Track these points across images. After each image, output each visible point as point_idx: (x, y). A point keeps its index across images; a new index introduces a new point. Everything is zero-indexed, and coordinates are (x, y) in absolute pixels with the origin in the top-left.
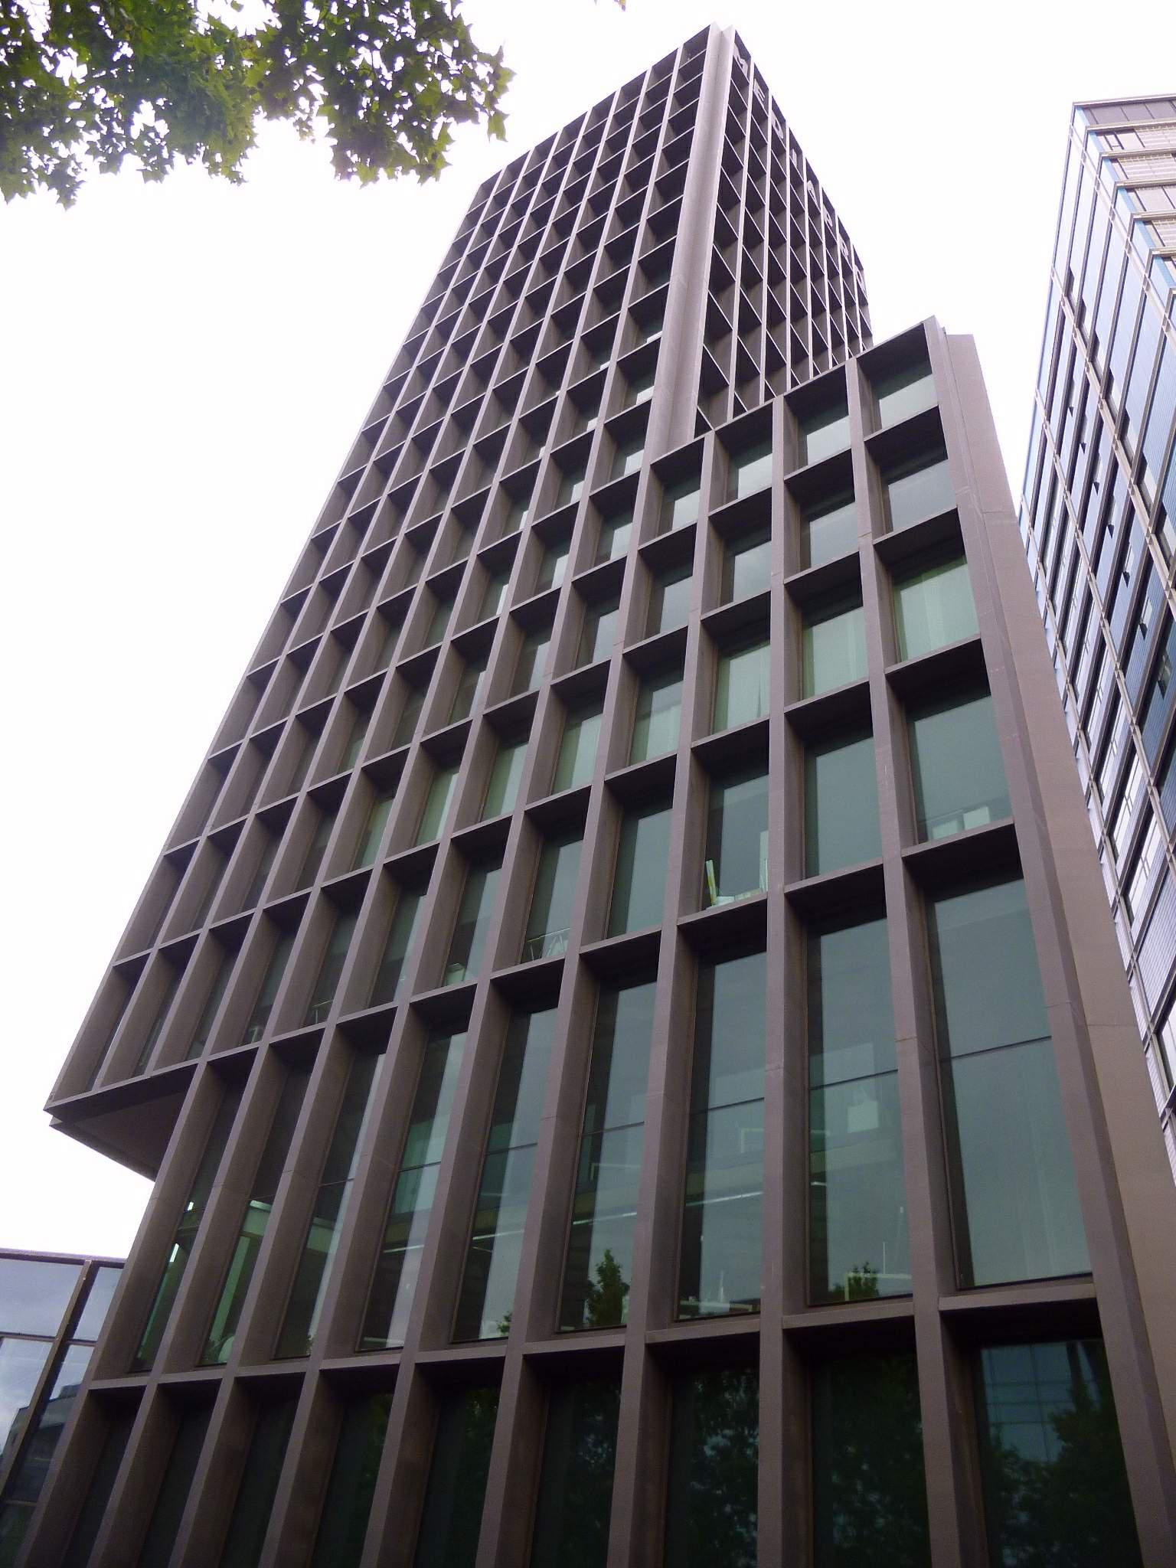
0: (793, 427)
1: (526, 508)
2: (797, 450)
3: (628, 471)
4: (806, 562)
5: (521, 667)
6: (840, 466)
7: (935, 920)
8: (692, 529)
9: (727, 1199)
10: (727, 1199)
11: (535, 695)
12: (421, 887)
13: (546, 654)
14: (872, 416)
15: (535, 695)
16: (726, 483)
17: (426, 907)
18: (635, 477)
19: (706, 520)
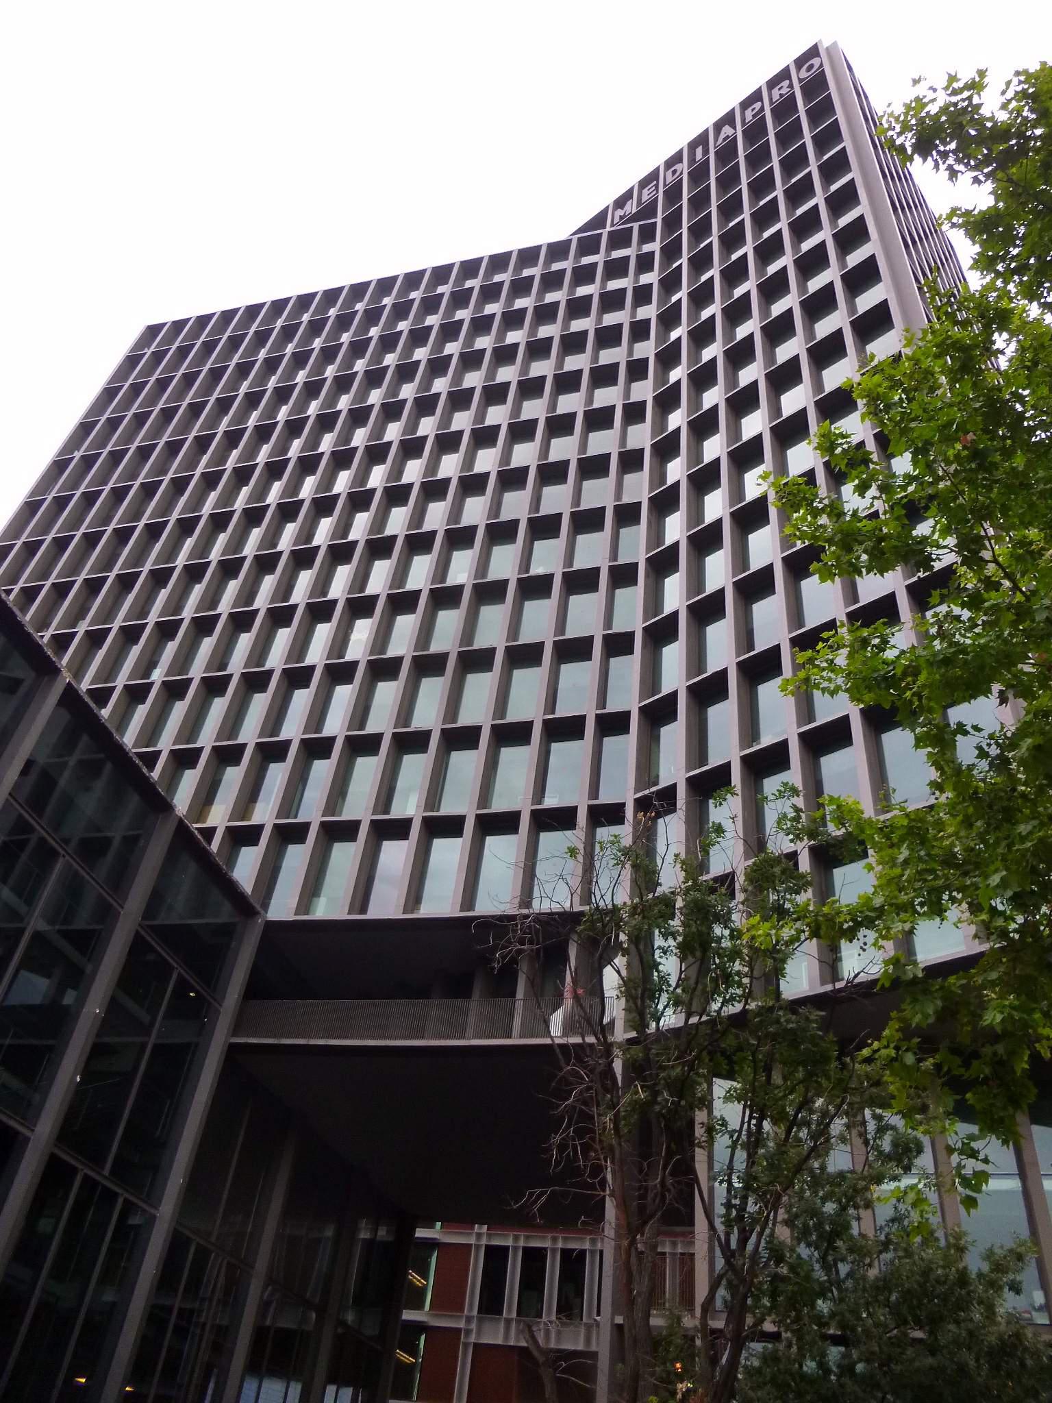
0: (726, 287)
1: (191, 536)
2: (810, 333)
3: (399, 329)
4: (497, 515)
5: (283, 448)
6: (800, 417)
7: (330, 853)
8: (677, 544)
9: (24, 1329)
10: (24, 1329)
11: (191, 679)
12: (135, 641)
13: (277, 488)
14: (852, 308)
15: (191, 679)
16: (732, 380)
17: (135, 651)
18: (401, 332)
19: (728, 515)
